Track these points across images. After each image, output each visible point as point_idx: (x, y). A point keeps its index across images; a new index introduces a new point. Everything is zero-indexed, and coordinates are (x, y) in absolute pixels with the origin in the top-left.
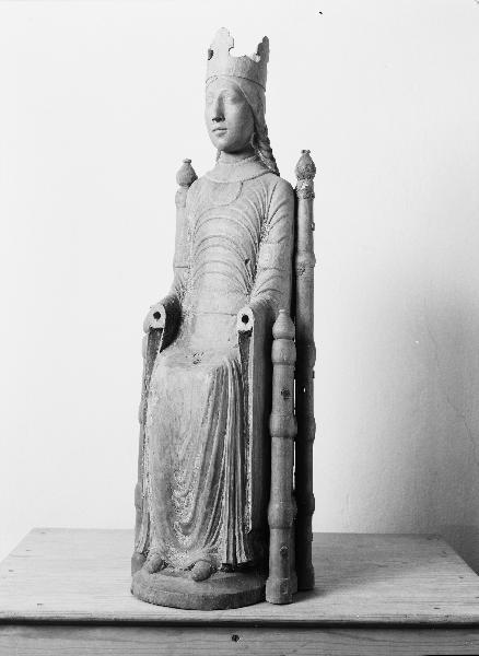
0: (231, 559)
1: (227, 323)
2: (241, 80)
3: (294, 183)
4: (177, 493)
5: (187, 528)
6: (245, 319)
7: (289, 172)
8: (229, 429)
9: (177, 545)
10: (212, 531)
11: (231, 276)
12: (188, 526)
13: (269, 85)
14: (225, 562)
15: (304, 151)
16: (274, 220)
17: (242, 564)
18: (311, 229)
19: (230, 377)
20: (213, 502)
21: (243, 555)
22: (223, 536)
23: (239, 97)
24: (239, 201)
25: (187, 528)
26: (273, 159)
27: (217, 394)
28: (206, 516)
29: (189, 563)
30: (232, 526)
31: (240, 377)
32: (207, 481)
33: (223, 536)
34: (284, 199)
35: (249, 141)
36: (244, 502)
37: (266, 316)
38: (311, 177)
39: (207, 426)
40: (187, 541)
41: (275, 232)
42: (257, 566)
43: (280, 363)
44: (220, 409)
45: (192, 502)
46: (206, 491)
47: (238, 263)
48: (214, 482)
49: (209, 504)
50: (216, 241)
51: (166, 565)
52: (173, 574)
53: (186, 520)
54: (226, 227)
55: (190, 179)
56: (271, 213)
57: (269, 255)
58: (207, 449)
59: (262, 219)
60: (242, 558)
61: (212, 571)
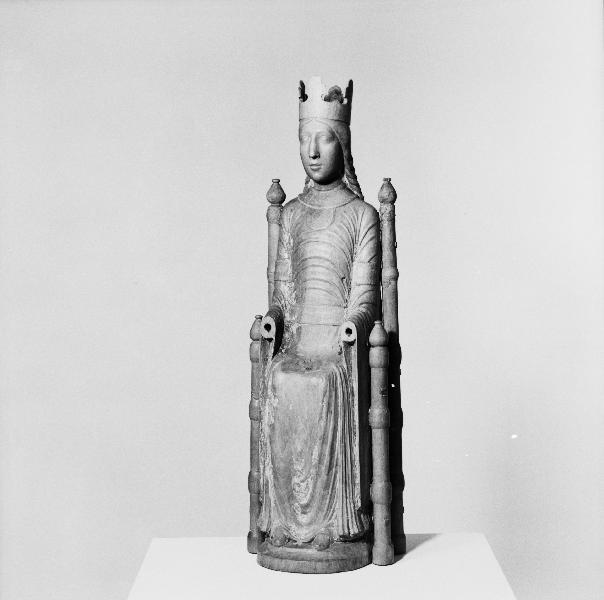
0: (346, 531)
1: (329, 332)
2: (337, 123)
3: (377, 205)
4: (296, 480)
5: (305, 508)
6: (349, 331)
7: (372, 193)
8: (340, 428)
9: (299, 524)
10: (330, 507)
11: (330, 292)
12: (307, 506)
13: (352, 124)
14: (341, 534)
15: (385, 180)
16: (365, 240)
17: (355, 535)
18: (394, 248)
19: (339, 381)
20: (329, 485)
21: (355, 527)
22: (338, 512)
23: (332, 137)
24: (334, 227)
25: (305, 508)
26: (358, 185)
27: (330, 396)
28: (323, 497)
29: (309, 537)
30: (345, 506)
31: (346, 381)
32: (324, 468)
33: (338, 512)
34: (370, 225)
35: (339, 171)
36: (354, 484)
37: (365, 325)
38: (393, 202)
39: (322, 424)
40: (303, 519)
41: (364, 253)
42: (367, 537)
43: (267, 315)
44: (332, 408)
45: (311, 486)
46: (324, 477)
47: (336, 281)
48: (330, 468)
49: (326, 487)
50: (316, 262)
51: (289, 539)
52: (297, 547)
53: (304, 501)
54: (323, 246)
55: (279, 200)
56: (362, 234)
57: (361, 272)
58: (324, 442)
59: (354, 242)
60: (354, 530)
61: (331, 542)
